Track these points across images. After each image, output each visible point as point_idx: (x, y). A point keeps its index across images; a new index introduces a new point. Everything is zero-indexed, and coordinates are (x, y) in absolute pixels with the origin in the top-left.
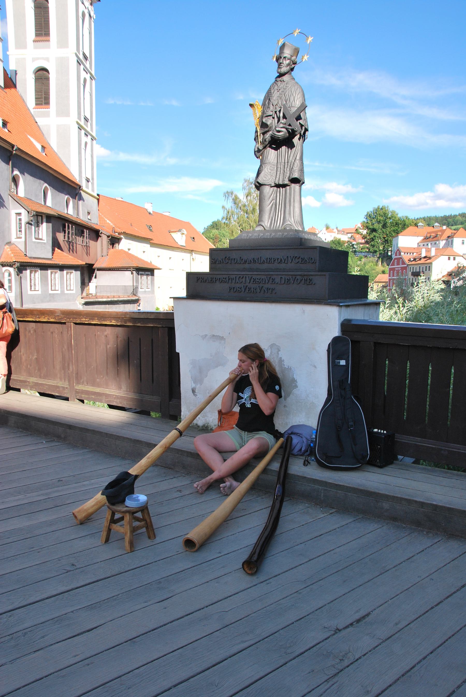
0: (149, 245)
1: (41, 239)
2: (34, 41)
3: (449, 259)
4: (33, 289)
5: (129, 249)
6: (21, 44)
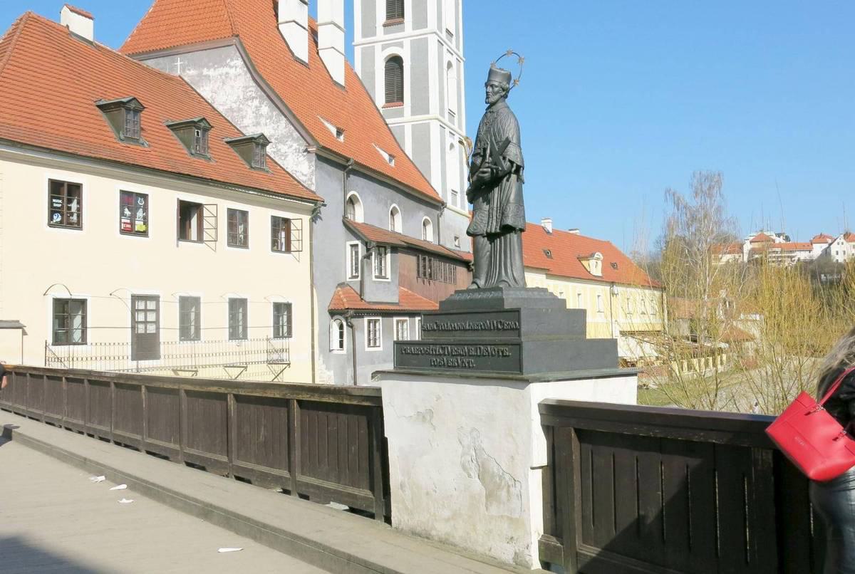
0: (545, 276)
1: (385, 278)
2: (385, 26)
3: (64, 203)
4: (372, 345)
5: (561, 293)
6: (369, 30)
